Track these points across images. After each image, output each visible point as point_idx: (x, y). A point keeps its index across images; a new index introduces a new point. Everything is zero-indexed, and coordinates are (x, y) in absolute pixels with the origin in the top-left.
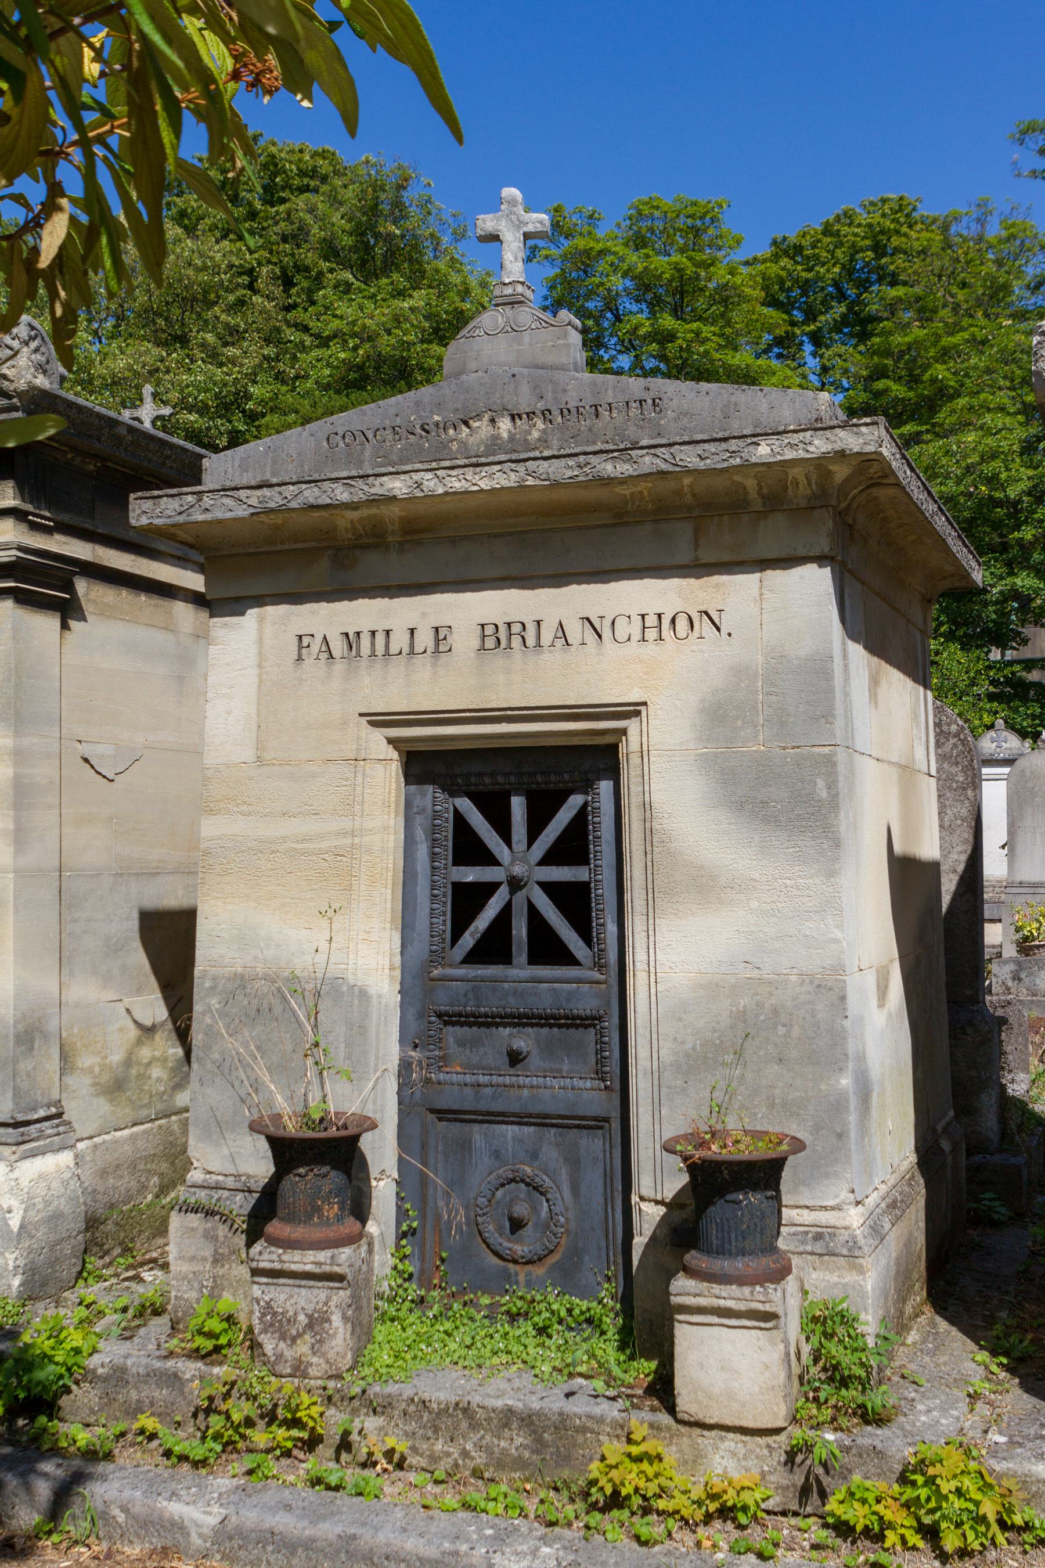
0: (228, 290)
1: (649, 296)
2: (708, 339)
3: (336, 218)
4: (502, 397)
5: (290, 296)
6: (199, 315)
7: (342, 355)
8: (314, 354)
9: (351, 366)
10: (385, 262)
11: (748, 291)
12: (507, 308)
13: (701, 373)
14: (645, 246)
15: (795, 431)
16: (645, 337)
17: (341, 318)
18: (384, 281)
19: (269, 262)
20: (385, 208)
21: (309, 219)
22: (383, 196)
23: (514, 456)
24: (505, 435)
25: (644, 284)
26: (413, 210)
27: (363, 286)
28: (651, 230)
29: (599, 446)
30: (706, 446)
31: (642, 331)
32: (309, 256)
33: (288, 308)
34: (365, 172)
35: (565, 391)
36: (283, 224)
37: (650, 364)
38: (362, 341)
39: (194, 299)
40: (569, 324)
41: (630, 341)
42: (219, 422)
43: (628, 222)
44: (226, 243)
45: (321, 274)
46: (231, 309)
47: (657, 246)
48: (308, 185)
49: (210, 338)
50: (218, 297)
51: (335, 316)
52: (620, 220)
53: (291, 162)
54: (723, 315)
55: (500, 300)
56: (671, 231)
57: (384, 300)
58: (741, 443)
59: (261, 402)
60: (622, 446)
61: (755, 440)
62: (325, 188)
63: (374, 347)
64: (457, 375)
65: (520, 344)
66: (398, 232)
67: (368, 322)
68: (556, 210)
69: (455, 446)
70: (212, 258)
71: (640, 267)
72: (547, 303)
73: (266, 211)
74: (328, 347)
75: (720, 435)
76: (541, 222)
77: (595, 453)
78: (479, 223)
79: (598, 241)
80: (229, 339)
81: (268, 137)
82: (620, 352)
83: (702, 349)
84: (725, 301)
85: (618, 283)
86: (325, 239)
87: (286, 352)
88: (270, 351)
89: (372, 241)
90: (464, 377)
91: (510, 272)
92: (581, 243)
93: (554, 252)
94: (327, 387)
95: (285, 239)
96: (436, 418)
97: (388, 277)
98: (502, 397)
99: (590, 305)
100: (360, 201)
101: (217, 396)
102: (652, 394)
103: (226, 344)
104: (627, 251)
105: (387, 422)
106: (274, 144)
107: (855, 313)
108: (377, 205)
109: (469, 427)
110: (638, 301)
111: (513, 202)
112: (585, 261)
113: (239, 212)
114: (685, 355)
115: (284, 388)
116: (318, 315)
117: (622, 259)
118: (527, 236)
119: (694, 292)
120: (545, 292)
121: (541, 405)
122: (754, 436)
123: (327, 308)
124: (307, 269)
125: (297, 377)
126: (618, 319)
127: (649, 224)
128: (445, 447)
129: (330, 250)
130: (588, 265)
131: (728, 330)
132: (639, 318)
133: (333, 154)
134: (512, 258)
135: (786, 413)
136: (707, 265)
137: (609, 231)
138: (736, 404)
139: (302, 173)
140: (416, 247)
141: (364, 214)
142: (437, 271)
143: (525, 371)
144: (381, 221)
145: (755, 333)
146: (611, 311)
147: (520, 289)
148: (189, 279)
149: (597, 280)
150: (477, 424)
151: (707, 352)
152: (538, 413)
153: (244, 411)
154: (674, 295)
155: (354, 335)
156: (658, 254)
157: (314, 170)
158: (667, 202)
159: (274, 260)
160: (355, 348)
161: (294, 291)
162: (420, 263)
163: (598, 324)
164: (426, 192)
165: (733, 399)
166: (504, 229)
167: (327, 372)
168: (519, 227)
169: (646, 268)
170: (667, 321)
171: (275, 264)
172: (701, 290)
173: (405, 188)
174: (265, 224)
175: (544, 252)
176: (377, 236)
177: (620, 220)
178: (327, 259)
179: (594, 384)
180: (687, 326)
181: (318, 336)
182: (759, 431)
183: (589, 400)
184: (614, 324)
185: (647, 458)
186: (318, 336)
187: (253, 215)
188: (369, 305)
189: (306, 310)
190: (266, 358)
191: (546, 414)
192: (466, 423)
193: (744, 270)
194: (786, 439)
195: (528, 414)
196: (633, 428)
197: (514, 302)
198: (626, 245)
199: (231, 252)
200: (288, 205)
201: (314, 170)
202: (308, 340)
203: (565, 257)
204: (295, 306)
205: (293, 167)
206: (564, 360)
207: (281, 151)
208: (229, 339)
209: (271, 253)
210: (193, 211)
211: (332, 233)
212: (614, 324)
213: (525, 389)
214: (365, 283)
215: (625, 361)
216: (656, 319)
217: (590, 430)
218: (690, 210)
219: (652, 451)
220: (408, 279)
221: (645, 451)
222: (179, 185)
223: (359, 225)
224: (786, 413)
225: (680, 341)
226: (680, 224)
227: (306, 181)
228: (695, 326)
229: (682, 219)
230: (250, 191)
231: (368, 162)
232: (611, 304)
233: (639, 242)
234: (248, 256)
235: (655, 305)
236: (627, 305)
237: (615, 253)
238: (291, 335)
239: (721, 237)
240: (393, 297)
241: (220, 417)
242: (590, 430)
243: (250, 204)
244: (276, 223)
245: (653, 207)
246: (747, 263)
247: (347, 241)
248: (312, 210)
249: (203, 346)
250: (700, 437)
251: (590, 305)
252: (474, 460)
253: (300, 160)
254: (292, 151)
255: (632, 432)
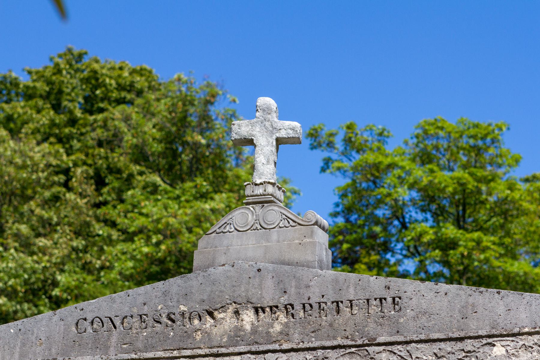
0: (43, 187)
1: (434, 207)
2: (488, 248)
3: (148, 127)
4: (247, 291)
5: (101, 195)
6: (16, 209)
7: (146, 250)
8: (119, 247)
9: (151, 260)
10: (190, 168)
11: (525, 205)
12: (258, 207)
13: (481, 279)
14: (430, 162)
15: (530, 334)
16: (429, 244)
17: (147, 216)
18: (188, 184)
19: (85, 163)
20: (193, 120)
21: (123, 127)
22: (192, 110)
23: (254, 348)
24: (248, 327)
25: (428, 196)
26: (218, 123)
27: (169, 188)
28: (436, 148)
29: (339, 341)
30: (442, 345)
31: (426, 239)
32: (120, 159)
33: (98, 205)
34: (175, 88)
35: (308, 287)
36: (99, 131)
37: (433, 268)
38: (165, 237)
39: (13, 194)
40: (316, 223)
41: (415, 247)
42: (26, 306)
43: (415, 140)
44: (46, 145)
45: (131, 176)
46: (48, 203)
47: (441, 162)
48: (125, 98)
49: (24, 229)
50: (35, 193)
51: (141, 214)
52: (408, 138)
53: (111, 78)
54: (502, 226)
55: (251, 199)
56: (455, 150)
57: (187, 201)
58: (477, 343)
59: (67, 289)
60: (359, 342)
61: (490, 340)
62: (139, 101)
63: (176, 243)
64: (205, 268)
65: (268, 241)
66: (203, 141)
67: (172, 220)
68: (348, 127)
69: (199, 336)
70: (31, 158)
71: (425, 181)
72: (339, 209)
73: (84, 119)
74: (133, 241)
75: (456, 335)
76: (293, 129)
77: (333, 348)
78: (235, 128)
79: (387, 156)
80: (41, 230)
81: (92, 55)
82: (405, 256)
83: (482, 257)
84: (505, 214)
85: (404, 194)
86: (136, 146)
87: (94, 244)
88: (79, 243)
89: (180, 149)
90: (211, 269)
91: (262, 174)
92: (371, 157)
93: (346, 164)
94: (128, 278)
95: (100, 144)
96: (183, 308)
97: (193, 181)
98: (247, 291)
99: (379, 213)
100: (170, 113)
101: (26, 282)
102: (392, 293)
103: (38, 235)
104: (413, 166)
105: (135, 310)
106: (97, 61)
107: (362, 170)
108: (185, 117)
109: (213, 317)
110: (423, 210)
111: (267, 110)
112: (375, 173)
113: (61, 119)
114: (466, 261)
115: (89, 278)
116: (126, 212)
117: (409, 173)
118: (279, 141)
119: (476, 204)
120: (336, 199)
121: (284, 300)
122: (489, 336)
123: (134, 206)
124: (119, 171)
125: (102, 268)
126: (404, 226)
127: (434, 142)
128: (189, 336)
129: (140, 156)
130: (377, 177)
131: (507, 240)
132: (424, 226)
133: (150, 72)
134: (264, 161)
135: (523, 316)
136: (487, 181)
137: (398, 147)
138: (473, 305)
139: (120, 87)
140: (220, 156)
141: (174, 124)
142: (238, 177)
143: (270, 266)
144: (189, 131)
145: (532, 244)
146: (398, 218)
147: (270, 189)
148: (9, 175)
149: (385, 191)
150: (222, 315)
151: (487, 260)
152: (281, 307)
153: (50, 298)
154: (457, 206)
155: (158, 232)
156: (442, 169)
157: (132, 85)
158: (451, 123)
159: (90, 162)
160: (158, 244)
161: (105, 190)
162: (223, 170)
163: (385, 229)
164: (232, 107)
165: (471, 300)
166: (258, 134)
167: (130, 264)
168: (272, 133)
169: (431, 182)
170: (450, 230)
171: (90, 166)
172: (483, 203)
173: (212, 103)
174: (84, 130)
175: (336, 164)
176: (185, 144)
177: (408, 138)
178: (137, 162)
179: (336, 281)
180: (468, 236)
181: (124, 232)
182: (494, 332)
183: (331, 296)
184: (400, 231)
185: (384, 355)
186: (124, 232)
187: (73, 122)
188: (173, 205)
189: (115, 207)
190: (75, 250)
191: (289, 308)
192: (211, 314)
193: (523, 186)
194: (521, 341)
195: (271, 308)
196: (372, 325)
197: (264, 202)
198: (413, 160)
199: (50, 153)
200: (105, 114)
201: (132, 85)
202: (115, 235)
203: (355, 169)
204: (105, 203)
205: (113, 82)
206: (310, 258)
207: (102, 68)
208: (41, 230)
209: (87, 155)
210: (19, 116)
211: (144, 141)
212: (400, 231)
213: (269, 283)
214: (171, 185)
215: (410, 265)
216: (440, 228)
217: (331, 325)
218: (472, 132)
219: (389, 348)
220: (211, 183)
221: (381, 348)
222: (9, 94)
223: (169, 133)
224: (523, 316)
225: (461, 249)
226: (463, 143)
227: (123, 94)
228: (476, 235)
229: (465, 139)
230: (72, 101)
231: (179, 80)
232: (398, 212)
233: (425, 158)
234: (65, 157)
235: (439, 215)
236: (413, 214)
237: (402, 168)
238: (100, 230)
239: (501, 156)
240: (196, 199)
241: (28, 301)
242: (331, 325)
243: (71, 112)
244: (94, 130)
245: (438, 127)
246: (527, 180)
247: (157, 148)
248: (127, 119)
249: (17, 236)
250: (436, 336)
251: (379, 213)
252: (215, 350)
253: (120, 76)
254: (113, 68)
255: (371, 328)
